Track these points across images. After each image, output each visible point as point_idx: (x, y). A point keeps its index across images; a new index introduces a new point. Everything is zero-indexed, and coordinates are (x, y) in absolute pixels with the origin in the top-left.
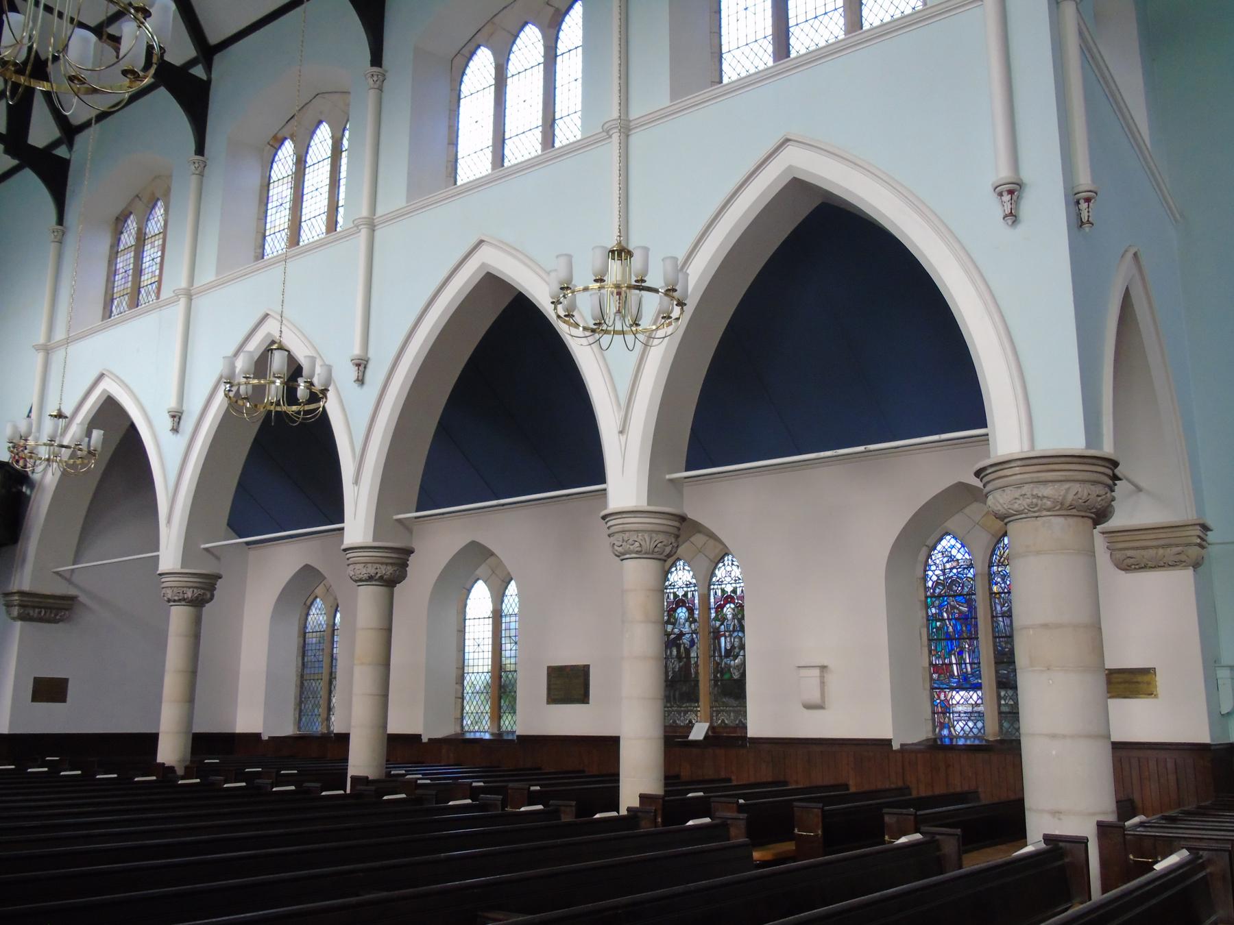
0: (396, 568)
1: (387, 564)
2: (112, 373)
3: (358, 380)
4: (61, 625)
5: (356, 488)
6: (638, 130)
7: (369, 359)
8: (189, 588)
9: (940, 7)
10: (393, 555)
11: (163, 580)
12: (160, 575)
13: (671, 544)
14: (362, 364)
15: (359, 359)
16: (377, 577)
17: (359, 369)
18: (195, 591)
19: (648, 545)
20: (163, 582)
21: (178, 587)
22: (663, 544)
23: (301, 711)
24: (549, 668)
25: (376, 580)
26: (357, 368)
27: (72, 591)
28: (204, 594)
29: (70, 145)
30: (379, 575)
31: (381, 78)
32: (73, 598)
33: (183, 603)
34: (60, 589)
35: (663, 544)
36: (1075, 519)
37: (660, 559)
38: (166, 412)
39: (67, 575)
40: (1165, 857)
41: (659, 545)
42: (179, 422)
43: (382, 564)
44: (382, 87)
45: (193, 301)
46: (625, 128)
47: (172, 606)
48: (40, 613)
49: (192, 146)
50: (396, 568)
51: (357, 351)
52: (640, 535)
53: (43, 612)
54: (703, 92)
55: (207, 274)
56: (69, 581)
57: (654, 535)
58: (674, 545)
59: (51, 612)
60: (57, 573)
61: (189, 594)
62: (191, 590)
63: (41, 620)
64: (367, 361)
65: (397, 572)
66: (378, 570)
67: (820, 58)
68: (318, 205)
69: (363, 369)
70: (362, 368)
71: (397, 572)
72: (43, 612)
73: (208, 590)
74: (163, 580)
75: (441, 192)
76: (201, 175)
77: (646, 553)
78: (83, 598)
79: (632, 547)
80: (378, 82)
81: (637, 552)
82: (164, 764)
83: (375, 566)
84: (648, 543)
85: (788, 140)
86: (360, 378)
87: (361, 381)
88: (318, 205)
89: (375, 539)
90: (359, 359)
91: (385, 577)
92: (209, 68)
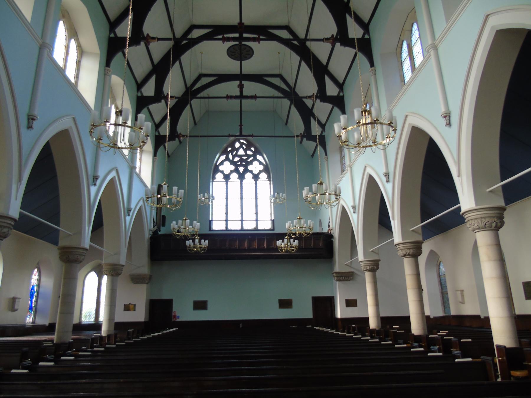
0: (414, 250)
1: (410, 249)
2: (369, 165)
3: (447, 125)
4: (350, 282)
5: (460, 178)
6: (439, 45)
7: (450, 112)
8: (368, 265)
9: (442, 35)
10: (370, 262)
11: (397, 247)
12: (396, 245)
13: (495, 221)
14: (447, 116)
15: (445, 114)
16: (407, 254)
17: (446, 119)
18: (370, 266)
19: (482, 225)
20: (397, 248)
21: (364, 266)
22: (489, 222)
23: (444, 306)
24: (357, 306)
25: (407, 256)
26: (445, 119)
27: (352, 270)
28: (374, 267)
29: (343, 92)
30: (407, 254)
31: (374, 71)
32: (352, 272)
33: (368, 271)
34: (348, 270)
35: (489, 222)
36: (489, 231)
37: (491, 230)
38: (382, 175)
39: (349, 265)
40: (240, 326)
41: (487, 224)
42: (355, 210)
43: (408, 249)
44: (375, 73)
45: (352, 168)
46: (435, 48)
47: (404, 258)
48: (343, 278)
49: (324, 154)
50: (414, 250)
51: (443, 110)
52: (476, 220)
53: (344, 278)
54: (450, 20)
55: (353, 157)
56: (350, 267)
57: (483, 219)
58: (497, 222)
59: (346, 278)
60: (346, 265)
61: (368, 268)
62: (369, 266)
63: (343, 280)
64: (450, 113)
65: (415, 251)
66: (407, 252)
67: (413, 80)
68: (408, 64)
69: (449, 118)
70: (447, 118)
71: (415, 251)
72: (344, 278)
73: (375, 266)
74: (397, 247)
75: (455, 13)
76: (375, 74)
77: (482, 229)
78: (355, 271)
79: (474, 227)
80: (373, 73)
81: (477, 229)
82: (414, 334)
83: (405, 250)
84: (481, 224)
85: (488, 15)
86: (448, 123)
87: (449, 124)
88: (408, 64)
89: (403, 240)
90: (445, 114)
91: (410, 254)
92: (369, 34)
